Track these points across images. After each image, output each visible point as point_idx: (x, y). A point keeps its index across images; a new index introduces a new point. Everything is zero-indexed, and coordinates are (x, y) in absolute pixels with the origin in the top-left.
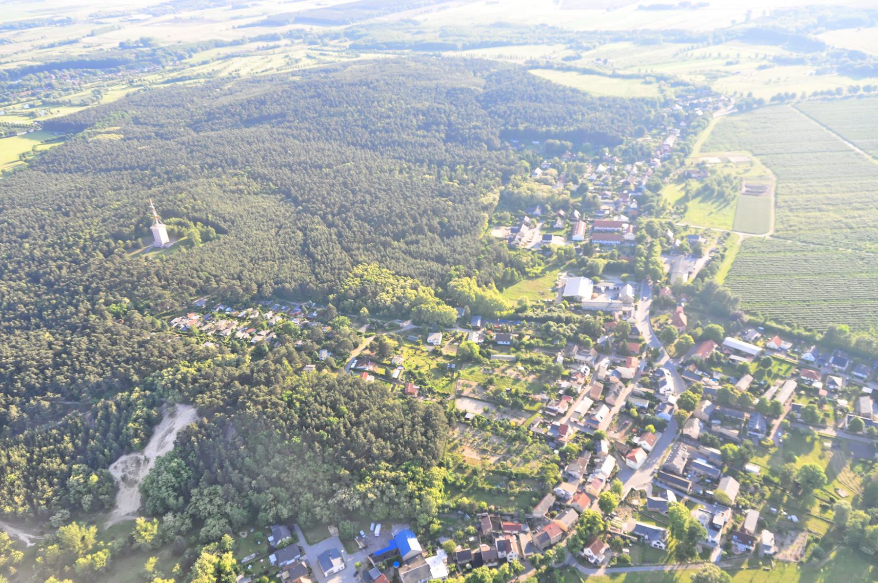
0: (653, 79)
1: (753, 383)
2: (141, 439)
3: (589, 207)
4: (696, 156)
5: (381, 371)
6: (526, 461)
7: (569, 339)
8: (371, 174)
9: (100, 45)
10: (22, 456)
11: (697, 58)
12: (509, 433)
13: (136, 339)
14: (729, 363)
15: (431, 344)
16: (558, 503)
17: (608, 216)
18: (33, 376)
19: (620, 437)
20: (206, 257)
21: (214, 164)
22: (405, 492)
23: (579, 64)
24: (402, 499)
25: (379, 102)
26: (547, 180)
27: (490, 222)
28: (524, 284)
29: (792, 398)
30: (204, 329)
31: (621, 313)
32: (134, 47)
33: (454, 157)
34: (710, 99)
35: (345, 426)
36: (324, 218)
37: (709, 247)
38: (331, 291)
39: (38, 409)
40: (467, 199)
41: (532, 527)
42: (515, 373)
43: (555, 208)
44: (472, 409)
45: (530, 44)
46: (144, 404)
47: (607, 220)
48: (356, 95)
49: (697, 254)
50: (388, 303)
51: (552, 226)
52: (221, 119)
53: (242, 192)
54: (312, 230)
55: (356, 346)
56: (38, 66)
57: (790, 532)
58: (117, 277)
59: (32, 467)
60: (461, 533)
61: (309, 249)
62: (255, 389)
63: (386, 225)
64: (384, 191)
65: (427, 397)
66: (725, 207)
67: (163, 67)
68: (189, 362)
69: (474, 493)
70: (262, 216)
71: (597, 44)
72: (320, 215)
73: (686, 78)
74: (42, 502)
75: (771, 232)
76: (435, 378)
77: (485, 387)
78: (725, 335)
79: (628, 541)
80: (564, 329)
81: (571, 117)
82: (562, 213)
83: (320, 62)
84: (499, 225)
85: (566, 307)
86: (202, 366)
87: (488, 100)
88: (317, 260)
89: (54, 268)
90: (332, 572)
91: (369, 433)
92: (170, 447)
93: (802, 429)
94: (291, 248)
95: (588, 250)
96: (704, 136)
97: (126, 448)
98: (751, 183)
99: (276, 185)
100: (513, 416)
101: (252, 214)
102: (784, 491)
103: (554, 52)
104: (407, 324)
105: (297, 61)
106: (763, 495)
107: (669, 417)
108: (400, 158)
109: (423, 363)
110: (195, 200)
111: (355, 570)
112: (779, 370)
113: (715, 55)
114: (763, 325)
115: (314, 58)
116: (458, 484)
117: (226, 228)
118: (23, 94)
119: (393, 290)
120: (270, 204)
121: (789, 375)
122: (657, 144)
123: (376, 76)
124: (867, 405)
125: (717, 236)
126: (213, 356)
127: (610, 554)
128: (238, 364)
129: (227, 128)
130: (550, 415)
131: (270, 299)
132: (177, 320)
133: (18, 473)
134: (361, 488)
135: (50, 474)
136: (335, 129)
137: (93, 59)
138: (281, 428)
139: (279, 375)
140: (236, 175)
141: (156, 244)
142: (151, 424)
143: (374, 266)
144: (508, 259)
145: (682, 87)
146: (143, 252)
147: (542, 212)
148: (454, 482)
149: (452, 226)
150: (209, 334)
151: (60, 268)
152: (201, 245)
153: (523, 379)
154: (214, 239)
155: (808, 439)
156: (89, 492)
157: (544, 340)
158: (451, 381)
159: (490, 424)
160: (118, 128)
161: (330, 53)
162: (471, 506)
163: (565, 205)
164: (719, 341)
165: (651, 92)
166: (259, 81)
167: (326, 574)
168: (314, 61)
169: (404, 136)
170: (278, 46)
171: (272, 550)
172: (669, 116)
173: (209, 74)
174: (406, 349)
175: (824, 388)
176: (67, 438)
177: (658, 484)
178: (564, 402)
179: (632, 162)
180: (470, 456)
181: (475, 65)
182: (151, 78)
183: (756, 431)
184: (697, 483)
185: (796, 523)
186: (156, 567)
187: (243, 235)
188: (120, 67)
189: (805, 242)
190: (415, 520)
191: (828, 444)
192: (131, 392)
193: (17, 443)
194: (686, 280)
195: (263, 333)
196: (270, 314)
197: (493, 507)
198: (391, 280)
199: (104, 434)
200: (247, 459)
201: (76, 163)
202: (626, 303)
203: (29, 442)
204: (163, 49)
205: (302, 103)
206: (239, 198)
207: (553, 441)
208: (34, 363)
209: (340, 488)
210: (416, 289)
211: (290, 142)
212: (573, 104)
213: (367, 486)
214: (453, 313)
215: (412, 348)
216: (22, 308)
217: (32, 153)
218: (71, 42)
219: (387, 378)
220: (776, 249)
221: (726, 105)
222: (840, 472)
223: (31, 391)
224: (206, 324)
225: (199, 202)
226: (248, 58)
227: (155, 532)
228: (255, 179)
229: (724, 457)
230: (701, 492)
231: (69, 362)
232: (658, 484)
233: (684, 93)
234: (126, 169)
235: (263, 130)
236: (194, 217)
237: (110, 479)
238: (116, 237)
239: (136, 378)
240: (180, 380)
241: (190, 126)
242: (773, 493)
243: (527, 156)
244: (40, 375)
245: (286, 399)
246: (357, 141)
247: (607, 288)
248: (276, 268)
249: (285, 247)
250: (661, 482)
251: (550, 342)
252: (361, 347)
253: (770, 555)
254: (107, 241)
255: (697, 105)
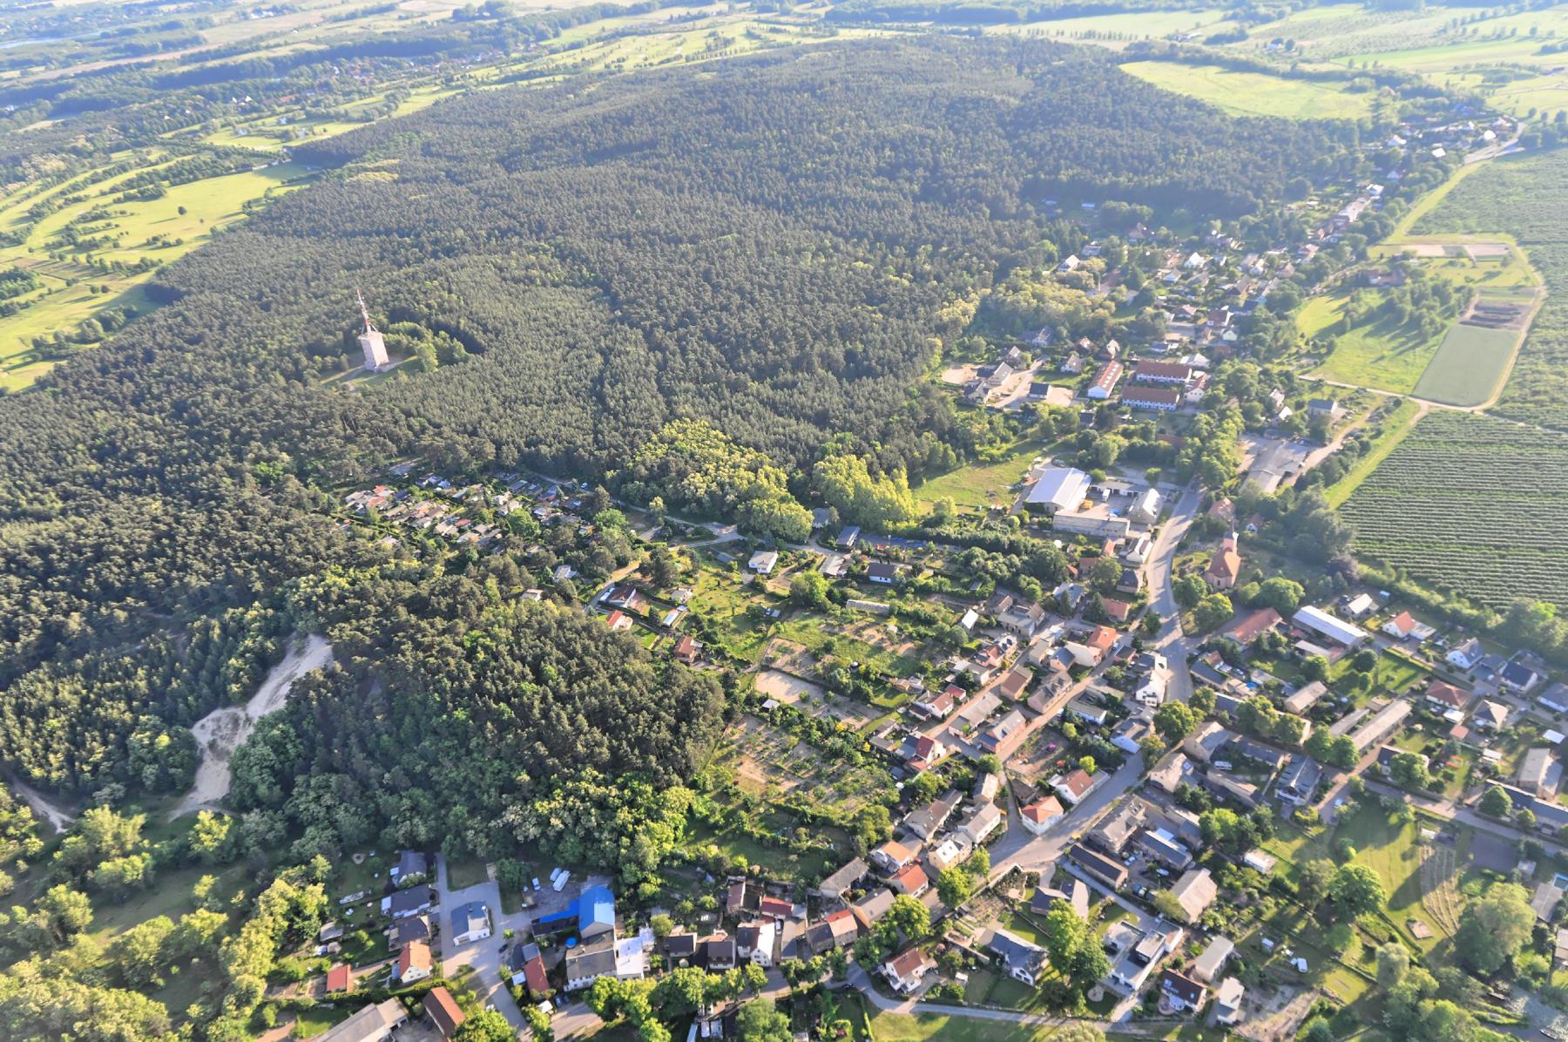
0: (1367, 82)
1: (1324, 698)
2: (244, 685)
3: (1141, 336)
4: (1399, 240)
5: (644, 610)
6: (843, 795)
7: (1001, 583)
8: (761, 254)
9: (424, 14)
10: (76, 693)
11: (1485, 39)
12: (829, 742)
13: (279, 522)
14: (1292, 655)
15: (754, 571)
16: (873, 876)
17: (1173, 354)
18: (116, 570)
19: (1028, 773)
20: (433, 392)
21: (509, 229)
22: (612, 824)
23: (1236, 50)
24: (606, 834)
25: (820, 122)
26: (1079, 279)
27: (946, 354)
28: (966, 475)
29: (1394, 736)
31: (1121, 541)
32: (474, 18)
33: (920, 230)
34: (1472, 125)
35: (544, 699)
36: (648, 335)
37: (1342, 426)
40: (914, 311)
41: (813, 913)
42: (879, 636)
43: (1076, 334)
44: (778, 690)
45: (1157, 10)
46: (260, 630)
47: (1168, 361)
48: (786, 111)
49: (1317, 438)
50: (701, 492)
51: (1058, 369)
52: (552, 149)
55: (622, 563)
56: (321, 52)
57: (1281, 988)
59: (87, 713)
60: (689, 905)
62: (424, 624)
63: (747, 351)
65: (711, 663)
66: (1413, 347)
67: (507, 54)
68: (344, 567)
69: (733, 839)
70: (550, 325)
71: (1288, 10)
72: (644, 329)
73: (1438, 80)
74: (86, 768)
75: (1491, 403)
76: (736, 631)
77: (815, 657)
78: (1304, 602)
79: (971, 961)
80: (999, 564)
81: (1165, 158)
82: (1086, 343)
83: (767, 44)
84: (963, 360)
85: (1023, 523)
86: (360, 576)
87: (1018, 122)
90: (467, 939)
91: (580, 716)
92: (281, 704)
93: (1385, 799)
94: (576, 384)
95: (1104, 420)
96: (1430, 202)
97: (220, 698)
98: (1489, 300)
99: (592, 270)
100: (850, 714)
102: (1303, 911)
103: (1198, 26)
104: (727, 533)
105: (727, 42)
106: (1258, 914)
107: (1134, 747)
109: (725, 603)
111: (504, 942)
112: (1389, 679)
113: (1524, 31)
114: (1389, 588)
115: (758, 37)
116: (712, 820)
118: (283, 100)
120: (571, 305)
121: (1405, 689)
122: (1326, 216)
123: (833, 75)
124: (1542, 765)
125: (1372, 406)
127: (932, 979)
128: (422, 575)
129: (559, 164)
130: (918, 718)
131: (514, 470)
133: (63, 718)
134: (542, 806)
135: (108, 725)
136: (731, 173)
137: (403, 39)
138: (442, 692)
140: (536, 250)
141: (367, 365)
142: (263, 665)
144: (947, 426)
145: (1421, 100)
147: (1050, 341)
148: (707, 817)
149: (867, 358)
150: (396, 523)
151: (216, 396)
153: (890, 649)
155: (1394, 819)
156: (155, 760)
157: (954, 579)
158: (761, 640)
159: (802, 722)
160: (396, 161)
161: (788, 28)
162: (718, 861)
163: (1097, 331)
164: (1288, 613)
165: (1353, 108)
166: (642, 81)
167: (456, 941)
168: (756, 43)
170: (705, 16)
171: (390, 890)
172: (1368, 158)
173: (575, 66)
174: (706, 576)
175: (1464, 724)
176: (141, 672)
177: (1068, 867)
178: (946, 697)
179: (1260, 250)
180: (749, 776)
181: (1023, 54)
182: (480, 73)
183: (1291, 791)
184: (1143, 873)
185: (1302, 974)
186: (214, 891)
188: (440, 55)
189: (1552, 427)
190: (620, 872)
191: (1429, 833)
193: (72, 672)
194: (1269, 488)
195: (481, 528)
197: (756, 869)
199: (195, 673)
200: (385, 737)
202: (1139, 523)
203: (89, 673)
204: (515, 22)
205: (692, 122)
207: (902, 767)
208: (121, 549)
209: (513, 804)
210: (755, 471)
212: (1178, 131)
213: (553, 804)
214: (805, 518)
215: (717, 575)
216: (142, 458)
218: (382, 10)
219: (651, 624)
220: (1485, 437)
221: (1502, 138)
222: (1433, 888)
223: (109, 593)
224: (395, 506)
225: (454, 297)
226: (649, 37)
227: (222, 836)
228: (563, 259)
229: (1205, 832)
230: (1142, 892)
231: (169, 552)
232: (1068, 867)
233: (1422, 112)
234: (378, 233)
235: (607, 171)
236: (437, 322)
237: (191, 743)
238: (313, 350)
239: (258, 586)
240: (320, 597)
241: (501, 160)
242: (1280, 913)
243: (1058, 232)
245: (468, 644)
246: (762, 196)
247: (1115, 493)
249: (566, 382)
250: (1074, 864)
251: (965, 586)
253: (1226, 1024)
255: (1438, 138)
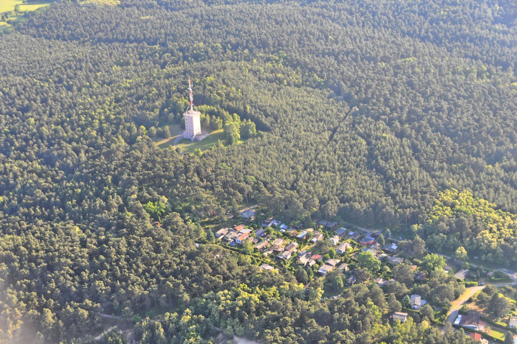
20: (249, 157)
30: (259, 246)
36: (390, 123)
38: (414, 219)
39: (75, 318)
53: (280, 82)
54: (377, 138)
55: (457, 296)
58: (151, 169)
61: (377, 161)
64: (465, 98)
70: (310, 114)
72: (385, 120)
86: (266, 293)
88: (391, 178)
89: (71, 151)
101: (298, 110)
108: (476, 58)
110: (228, 85)
117: (268, 124)
119: (499, 230)
126: (279, 284)
131: (332, 220)
132: (223, 231)
136: (384, 14)
139: (368, 319)
140: (268, 60)
141: (185, 134)
143: (466, 195)
146: (172, 143)
150: (266, 254)
151: (77, 151)
152: (239, 142)
154: (253, 136)
169: (477, 30)
187: (290, 136)
192: (181, 313)
195: (333, 262)
196: (336, 239)
198: (494, 215)
201: (70, 29)
206: (279, 89)
211: (329, 25)
216: (39, 194)
217: (14, 14)
224: (260, 241)
225: (234, 89)
228: (294, 67)
239: (186, 297)
244: (77, 277)
246: (415, 31)
248: (338, 182)
249: (345, 156)
252: (464, 298)
254: (128, 124)
